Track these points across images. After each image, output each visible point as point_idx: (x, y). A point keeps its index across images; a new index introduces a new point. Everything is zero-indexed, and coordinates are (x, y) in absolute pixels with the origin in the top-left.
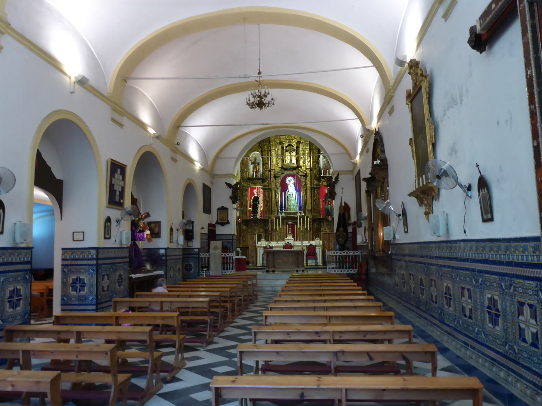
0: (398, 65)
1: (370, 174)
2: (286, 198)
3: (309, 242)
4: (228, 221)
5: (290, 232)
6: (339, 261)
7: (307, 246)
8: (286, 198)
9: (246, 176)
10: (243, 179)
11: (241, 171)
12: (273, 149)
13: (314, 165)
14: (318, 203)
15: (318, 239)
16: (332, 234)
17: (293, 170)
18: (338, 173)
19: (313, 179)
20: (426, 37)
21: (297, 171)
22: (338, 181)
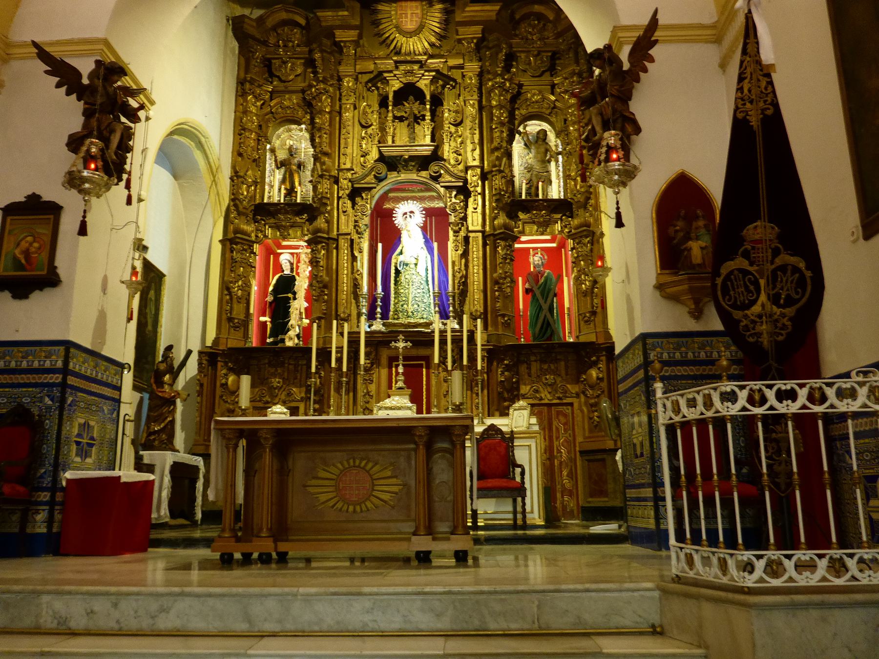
2: (393, 275)
4: (52, 269)
5: (400, 384)
6: (183, 592)
8: (393, 275)
10: (235, 205)
11: (231, 179)
13: (493, 157)
14: (508, 290)
15: (521, 408)
16: (560, 408)
17: (419, 171)
19: (492, 209)
22: (652, 60)
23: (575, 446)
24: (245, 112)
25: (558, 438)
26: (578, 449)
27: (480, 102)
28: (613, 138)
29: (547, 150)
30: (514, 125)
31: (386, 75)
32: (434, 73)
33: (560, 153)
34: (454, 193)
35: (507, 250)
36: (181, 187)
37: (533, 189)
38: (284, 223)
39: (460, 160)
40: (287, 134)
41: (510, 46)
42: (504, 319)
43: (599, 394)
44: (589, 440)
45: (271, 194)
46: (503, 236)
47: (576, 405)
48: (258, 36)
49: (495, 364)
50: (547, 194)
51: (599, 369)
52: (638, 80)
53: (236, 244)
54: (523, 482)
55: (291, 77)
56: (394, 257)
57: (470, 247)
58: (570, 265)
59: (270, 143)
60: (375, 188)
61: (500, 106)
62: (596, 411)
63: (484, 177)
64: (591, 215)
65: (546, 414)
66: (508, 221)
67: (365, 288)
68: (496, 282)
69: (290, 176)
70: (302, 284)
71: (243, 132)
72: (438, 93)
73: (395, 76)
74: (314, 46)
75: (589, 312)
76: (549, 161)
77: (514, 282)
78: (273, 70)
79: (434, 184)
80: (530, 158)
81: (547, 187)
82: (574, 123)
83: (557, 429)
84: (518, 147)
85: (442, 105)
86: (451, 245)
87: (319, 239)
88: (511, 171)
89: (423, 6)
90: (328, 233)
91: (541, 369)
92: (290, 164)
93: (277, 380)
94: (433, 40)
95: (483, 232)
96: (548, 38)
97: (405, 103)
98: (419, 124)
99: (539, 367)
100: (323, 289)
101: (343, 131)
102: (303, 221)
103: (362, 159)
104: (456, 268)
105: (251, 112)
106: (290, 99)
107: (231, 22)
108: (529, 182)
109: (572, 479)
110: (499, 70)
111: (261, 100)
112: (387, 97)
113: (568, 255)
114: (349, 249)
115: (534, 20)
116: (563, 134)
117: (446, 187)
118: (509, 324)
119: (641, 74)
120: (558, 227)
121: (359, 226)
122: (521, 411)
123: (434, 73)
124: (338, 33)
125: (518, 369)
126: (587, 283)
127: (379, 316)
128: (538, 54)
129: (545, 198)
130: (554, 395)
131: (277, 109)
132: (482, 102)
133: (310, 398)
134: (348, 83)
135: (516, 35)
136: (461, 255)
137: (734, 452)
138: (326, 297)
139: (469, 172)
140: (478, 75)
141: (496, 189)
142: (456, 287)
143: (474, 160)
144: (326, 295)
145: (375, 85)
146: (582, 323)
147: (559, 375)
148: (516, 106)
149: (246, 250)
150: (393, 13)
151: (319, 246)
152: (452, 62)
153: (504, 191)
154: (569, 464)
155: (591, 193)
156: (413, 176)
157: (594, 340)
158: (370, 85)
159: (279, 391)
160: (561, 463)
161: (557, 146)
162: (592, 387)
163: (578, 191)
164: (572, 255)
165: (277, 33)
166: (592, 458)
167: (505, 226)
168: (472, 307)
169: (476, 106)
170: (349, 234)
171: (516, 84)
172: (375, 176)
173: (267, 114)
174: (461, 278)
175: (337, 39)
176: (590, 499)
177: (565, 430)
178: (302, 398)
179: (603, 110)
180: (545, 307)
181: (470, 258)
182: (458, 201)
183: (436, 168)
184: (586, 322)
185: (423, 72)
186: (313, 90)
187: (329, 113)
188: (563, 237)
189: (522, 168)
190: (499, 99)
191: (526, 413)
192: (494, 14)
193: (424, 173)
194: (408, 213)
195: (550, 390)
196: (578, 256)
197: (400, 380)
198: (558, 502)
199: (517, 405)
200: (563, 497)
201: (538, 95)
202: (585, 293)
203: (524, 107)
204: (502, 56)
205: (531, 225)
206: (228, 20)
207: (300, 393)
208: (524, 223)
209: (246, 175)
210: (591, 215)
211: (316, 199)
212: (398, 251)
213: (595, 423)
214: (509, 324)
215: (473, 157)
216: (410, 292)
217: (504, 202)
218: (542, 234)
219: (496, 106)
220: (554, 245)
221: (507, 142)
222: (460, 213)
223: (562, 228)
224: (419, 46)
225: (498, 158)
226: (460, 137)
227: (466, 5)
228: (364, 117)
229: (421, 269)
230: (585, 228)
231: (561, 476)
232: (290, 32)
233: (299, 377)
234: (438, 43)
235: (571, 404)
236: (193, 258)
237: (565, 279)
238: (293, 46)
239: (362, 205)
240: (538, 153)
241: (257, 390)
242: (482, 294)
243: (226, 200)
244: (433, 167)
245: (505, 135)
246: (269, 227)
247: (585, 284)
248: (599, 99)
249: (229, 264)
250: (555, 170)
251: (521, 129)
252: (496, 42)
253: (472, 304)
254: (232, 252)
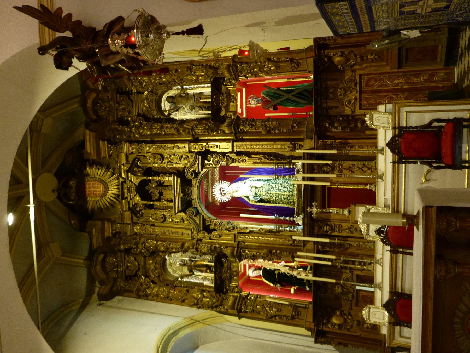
3: (382, 151)
5: (346, 212)
7: (394, 163)
13: (183, 133)
15: (372, 119)
16: (363, 84)
19: (218, 135)
23: (394, 72)
24: (157, 295)
25: (387, 86)
26: (396, 70)
27: (147, 142)
28: (116, 42)
29: (180, 96)
30: (163, 119)
31: (131, 206)
32: (129, 174)
33: (182, 87)
34: (206, 162)
35: (246, 124)
36: (204, 343)
37: (206, 105)
38: (228, 275)
39: (186, 156)
40: (173, 266)
41: (114, 122)
42: (296, 127)
43: (354, 54)
44: (390, 62)
45: (210, 278)
46: (236, 127)
47: (361, 72)
48: (110, 285)
49: (328, 133)
50: (208, 95)
51: (334, 55)
53: (241, 309)
54: (448, 121)
55: (136, 263)
56: (251, 203)
57: (243, 150)
58: (257, 78)
59: (177, 279)
60: (203, 216)
61: (151, 129)
62: (367, 57)
63: (196, 140)
64: (222, 64)
65: (367, 95)
66: (226, 124)
67: (272, 227)
68: (269, 132)
69: (198, 267)
70: (269, 265)
71: (169, 298)
72: (143, 170)
73: (131, 199)
74: (116, 249)
75: (291, 63)
76: (188, 94)
77: (269, 119)
78: (132, 275)
79: (200, 176)
80: (186, 107)
81: (204, 96)
82: (161, 78)
83: (379, 86)
84: (178, 116)
85: (151, 168)
86: (242, 165)
87: (238, 254)
88: (193, 121)
89: (88, 180)
90: (235, 247)
91: (333, 99)
92: (191, 266)
93: (336, 289)
94: (109, 173)
95: (233, 141)
96: (108, 97)
97: (150, 191)
99: (331, 101)
100: (272, 254)
102: (227, 262)
103: (185, 222)
104: (258, 161)
105: (157, 291)
106: (150, 265)
107: (102, 302)
108: (201, 108)
109: (421, 74)
110: (127, 129)
111: (150, 284)
112: (145, 205)
113: (251, 80)
114: (244, 234)
115: (97, 106)
116: (169, 85)
117: (203, 167)
118: (299, 123)
119: (74, 19)
120: (231, 88)
121: (229, 228)
122: (374, 118)
123: (129, 174)
124: (107, 235)
125: (332, 116)
126: (270, 66)
127: (292, 219)
128: (118, 103)
129: (210, 97)
130: (353, 89)
131: (156, 273)
132: (148, 141)
133: (350, 268)
134: (137, 229)
135: (107, 118)
136: (249, 158)
137: (314, 153)
138: (278, 251)
139: (193, 150)
140: (131, 144)
141: (204, 132)
142: (272, 161)
143: (184, 147)
144: (276, 251)
145: (139, 212)
146: (299, 69)
147: (338, 85)
148: (152, 117)
149: (245, 303)
150: (93, 199)
151: (243, 254)
152: (124, 161)
153: (205, 126)
154: (408, 76)
155: (207, 65)
156: (195, 189)
157: (312, 59)
158: (138, 215)
159: (345, 288)
160: (406, 83)
161: (178, 89)
162: (348, 60)
163: (206, 74)
164: (250, 77)
165: (109, 271)
166: (404, 60)
167: (229, 126)
168: (286, 150)
169: (150, 145)
170: (235, 235)
171: (137, 118)
172: (195, 216)
173: (160, 280)
174: (265, 158)
175: (111, 235)
176: (439, 60)
177: (380, 80)
178: (350, 272)
179: (103, 54)
180: (287, 96)
181: (251, 151)
182: (212, 159)
183: (189, 174)
184: (298, 66)
185: (128, 181)
186: (143, 251)
187: (157, 241)
188: (238, 84)
189: (192, 113)
190: (146, 129)
191: (376, 115)
192: (91, 133)
193: (193, 182)
194: (221, 192)
195: (349, 92)
196: (251, 73)
197: (343, 213)
198: (439, 85)
199: (368, 123)
200: (435, 81)
201: (144, 102)
202: (278, 67)
203: (152, 112)
204: (120, 127)
205: (230, 106)
206: (100, 305)
207: (346, 273)
208: (228, 112)
210: (222, 64)
211: (212, 254)
212: (246, 199)
213: (376, 57)
214: (299, 123)
215: (183, 148)
216: (275, 192)
217: (213, 126)
218: (236, 99)
219: (150, 131)
220: (244, 90)
221: (173, 124)
222: (220, 158)
223: (231, 85)
224: (114, 182)
225: (184, 131)
226: (170, 156)
227: (87, 152)
228: (159, 219)
229: (259, 184)
230: (231, 68)
231: (418, 83)
232: (109, 264)
233: (334, 273)
234: (112, 170)
235: (361, 76)
236: (252, 337)
237: (267, 82)
238: (117, 262)
239: (215, 225)
240: (182, 102)
241: (343, 302)
242: (277, 143)
244: (189, 176)
245: (169, 125)
246: (231, 284)
247: (271, 67)
248: (97, 59)
249: (254, 315)
250: (194, 90)
251: (166, 114)
252: (111, 132)
253: (284, 150)
254: (247, 312)
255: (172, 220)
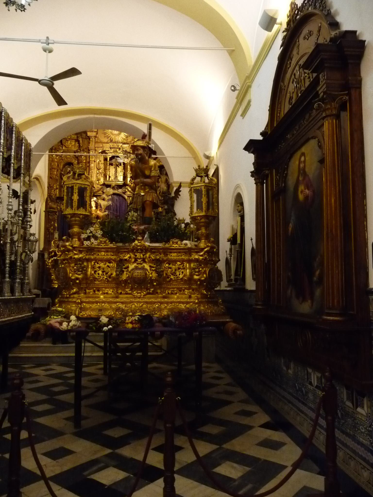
0: (264, 29)
1: (262, 134)
9: (56, 194)
10: (50, 198)
12: (93, 160)
17: (118, 189)
18: (179, 184)
20: (222, 145)
21: (124, 189)
22: (180, 195)
52: (176, 200)
98: (118, 167)
101: (90, 171)
103: (97, 182)
105: (55, 161)
117: (128, 196)
119: (177, 198)
149: (54, 215)
187: (85, 162)
209: (53, 186)
243: (46, 196)
255: (98, 174)
